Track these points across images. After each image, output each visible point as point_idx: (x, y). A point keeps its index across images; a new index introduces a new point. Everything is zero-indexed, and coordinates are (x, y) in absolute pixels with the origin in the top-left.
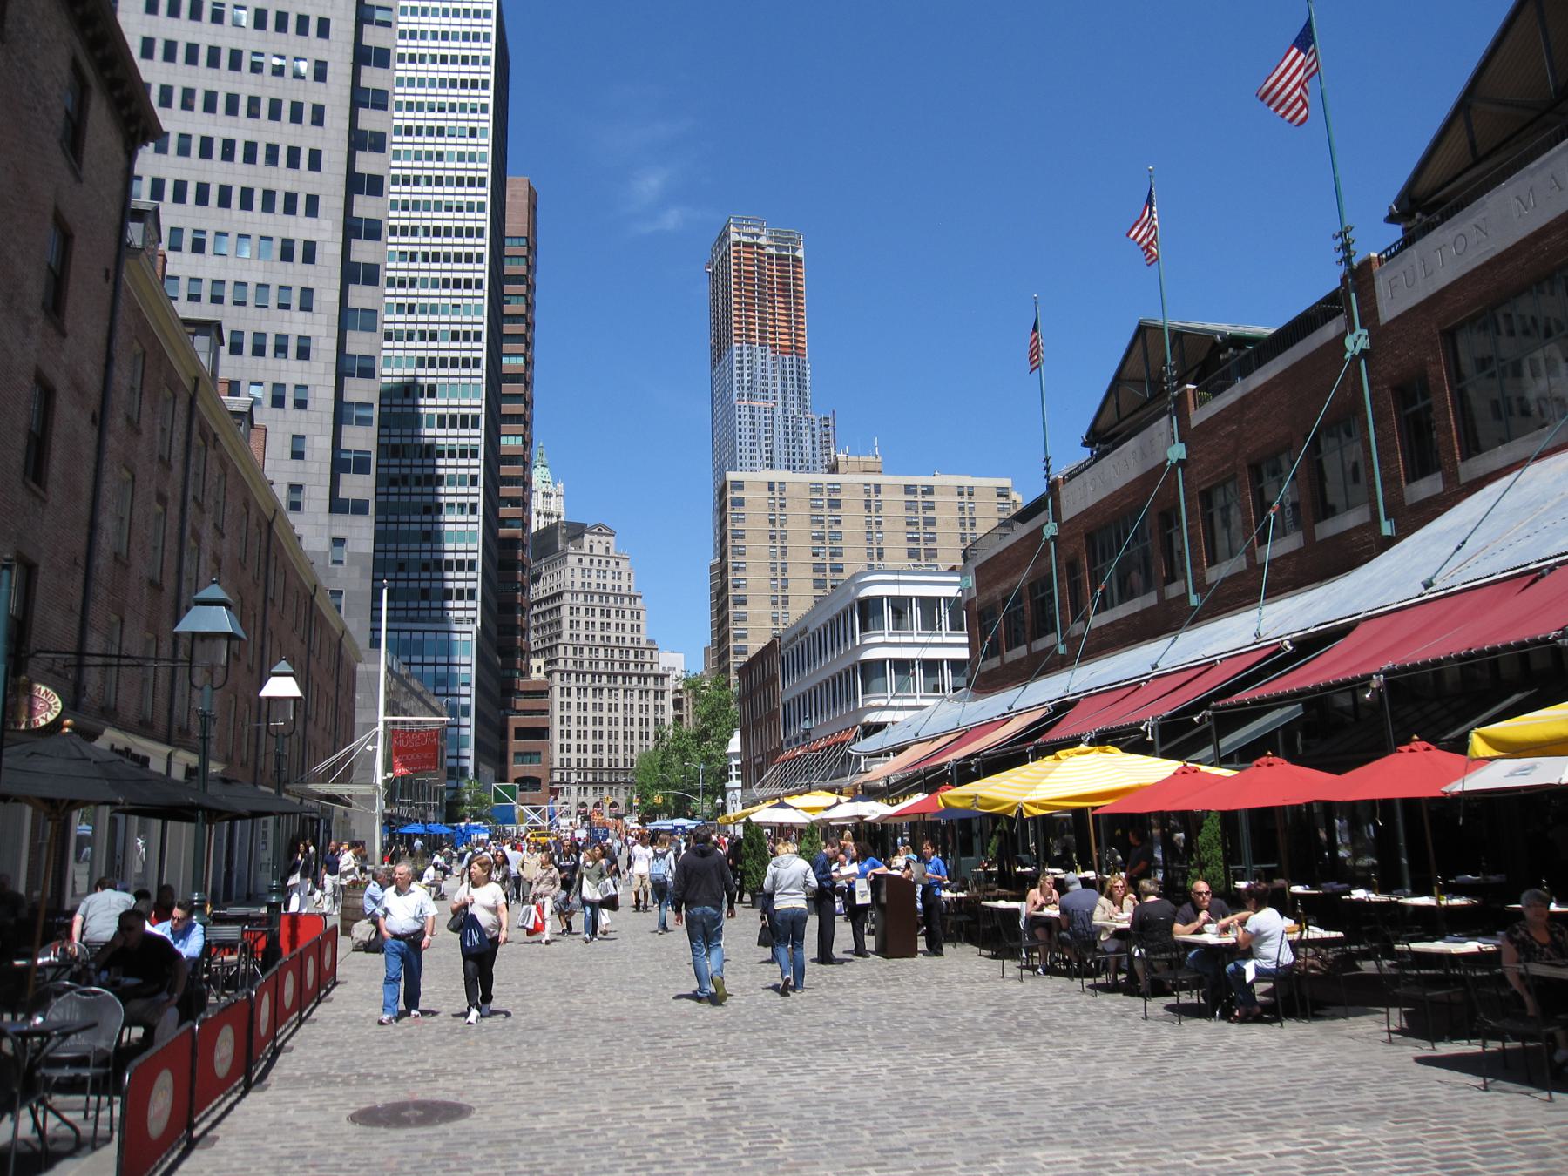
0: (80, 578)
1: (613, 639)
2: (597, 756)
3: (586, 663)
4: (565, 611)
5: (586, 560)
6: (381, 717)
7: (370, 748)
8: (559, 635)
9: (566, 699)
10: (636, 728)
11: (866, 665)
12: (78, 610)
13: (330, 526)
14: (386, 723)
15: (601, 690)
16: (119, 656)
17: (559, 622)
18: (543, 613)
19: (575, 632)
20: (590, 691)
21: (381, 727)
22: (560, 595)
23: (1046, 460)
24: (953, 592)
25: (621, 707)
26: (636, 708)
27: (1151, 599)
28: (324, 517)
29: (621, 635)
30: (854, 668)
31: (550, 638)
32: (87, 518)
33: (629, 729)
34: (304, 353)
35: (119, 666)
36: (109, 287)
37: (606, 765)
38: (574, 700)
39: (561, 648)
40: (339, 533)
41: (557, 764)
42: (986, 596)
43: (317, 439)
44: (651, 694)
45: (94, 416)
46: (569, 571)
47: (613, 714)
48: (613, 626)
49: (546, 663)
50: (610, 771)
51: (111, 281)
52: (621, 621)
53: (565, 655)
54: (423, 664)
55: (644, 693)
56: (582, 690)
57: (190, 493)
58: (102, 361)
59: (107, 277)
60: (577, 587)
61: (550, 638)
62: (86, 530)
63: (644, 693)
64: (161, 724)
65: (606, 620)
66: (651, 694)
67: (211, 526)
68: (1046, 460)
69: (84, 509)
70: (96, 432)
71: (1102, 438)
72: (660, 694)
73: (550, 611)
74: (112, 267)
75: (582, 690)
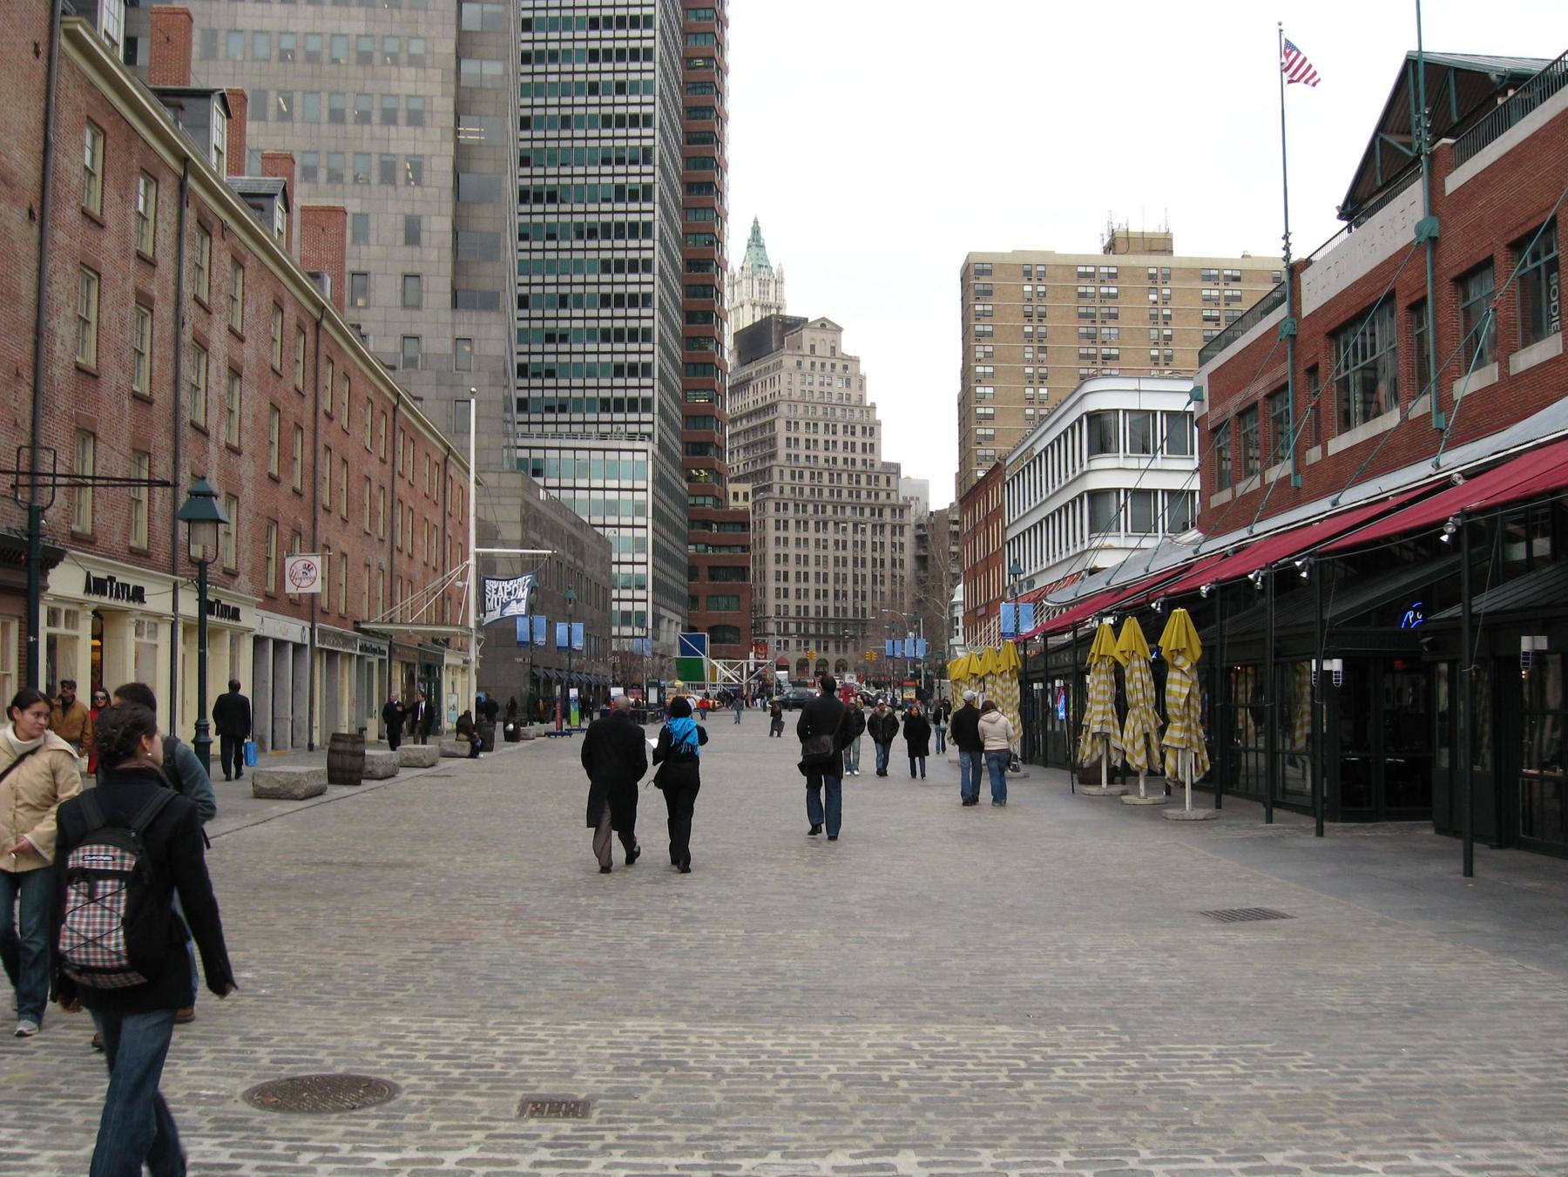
0: (26, 391)
1: (840, 462)
2: (802, 603)
3: (845, 493)
4: (780, 426)
5: (807, 364)
6: (473, 548)
7: (459, 584)
8: (773, 456)
9: (782, 534)
10: (868, 571)
11: (1096, 496)
12: (27, 427)
13: (453, 324)
14: (477, 555)
15: (825, 524)
16: (94, 478)
17: (772, 442)
18: (754, 429)
19: (793, 452)
20: (812, 524)
21: (472, 561)
22: (772, 407)
23: (1286, 237)
24: (1179, 404)
25: (850, 544)
26: (869, 546)
27: (1390, 420)
28: (446, 315)
29: (850, 456)
30: (1081, 497)
31: (763, 459)
32: (32, 324)
33: (859, 571)
34: (416, 119)
35: (54, 485)
36: (42, 63)
37: (831, 614)
38: (792, 534)
39: (776, 471)
40: (462, 332)
41: (771, 612)
42: (1218, 411)
43: (434, 219)
44: (888, 530)
45: (31, 212)
46: (784, 377)
47: (841, 553)
48: (840, 445)
49: (755, 492)
50: (837, 622)
51: (43, 55)
52: (850, 439)
53: (781, 481)
54: (575, 488)
55: (879, 528)
56: (802, 524)
57: (187, 290)
58: (41, 147)
59: (37, 53)
60: (796, 395)
61: (763, 459)
62: (31, 336)
63: (879, 528)
64: (162, 555)
65: (831, 438)
66: (888, 530)
67: (224, 329)
68: (1286, 237)
69: (26, 313)
70: (35, 229)
71: (1356, 208)
72: (898, 529)
73: (763, 426)
74: (42, 39)
75: (802, 524)
